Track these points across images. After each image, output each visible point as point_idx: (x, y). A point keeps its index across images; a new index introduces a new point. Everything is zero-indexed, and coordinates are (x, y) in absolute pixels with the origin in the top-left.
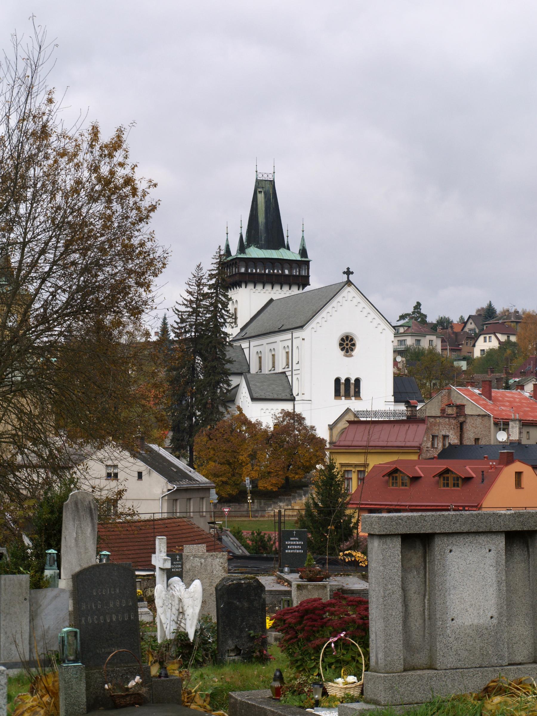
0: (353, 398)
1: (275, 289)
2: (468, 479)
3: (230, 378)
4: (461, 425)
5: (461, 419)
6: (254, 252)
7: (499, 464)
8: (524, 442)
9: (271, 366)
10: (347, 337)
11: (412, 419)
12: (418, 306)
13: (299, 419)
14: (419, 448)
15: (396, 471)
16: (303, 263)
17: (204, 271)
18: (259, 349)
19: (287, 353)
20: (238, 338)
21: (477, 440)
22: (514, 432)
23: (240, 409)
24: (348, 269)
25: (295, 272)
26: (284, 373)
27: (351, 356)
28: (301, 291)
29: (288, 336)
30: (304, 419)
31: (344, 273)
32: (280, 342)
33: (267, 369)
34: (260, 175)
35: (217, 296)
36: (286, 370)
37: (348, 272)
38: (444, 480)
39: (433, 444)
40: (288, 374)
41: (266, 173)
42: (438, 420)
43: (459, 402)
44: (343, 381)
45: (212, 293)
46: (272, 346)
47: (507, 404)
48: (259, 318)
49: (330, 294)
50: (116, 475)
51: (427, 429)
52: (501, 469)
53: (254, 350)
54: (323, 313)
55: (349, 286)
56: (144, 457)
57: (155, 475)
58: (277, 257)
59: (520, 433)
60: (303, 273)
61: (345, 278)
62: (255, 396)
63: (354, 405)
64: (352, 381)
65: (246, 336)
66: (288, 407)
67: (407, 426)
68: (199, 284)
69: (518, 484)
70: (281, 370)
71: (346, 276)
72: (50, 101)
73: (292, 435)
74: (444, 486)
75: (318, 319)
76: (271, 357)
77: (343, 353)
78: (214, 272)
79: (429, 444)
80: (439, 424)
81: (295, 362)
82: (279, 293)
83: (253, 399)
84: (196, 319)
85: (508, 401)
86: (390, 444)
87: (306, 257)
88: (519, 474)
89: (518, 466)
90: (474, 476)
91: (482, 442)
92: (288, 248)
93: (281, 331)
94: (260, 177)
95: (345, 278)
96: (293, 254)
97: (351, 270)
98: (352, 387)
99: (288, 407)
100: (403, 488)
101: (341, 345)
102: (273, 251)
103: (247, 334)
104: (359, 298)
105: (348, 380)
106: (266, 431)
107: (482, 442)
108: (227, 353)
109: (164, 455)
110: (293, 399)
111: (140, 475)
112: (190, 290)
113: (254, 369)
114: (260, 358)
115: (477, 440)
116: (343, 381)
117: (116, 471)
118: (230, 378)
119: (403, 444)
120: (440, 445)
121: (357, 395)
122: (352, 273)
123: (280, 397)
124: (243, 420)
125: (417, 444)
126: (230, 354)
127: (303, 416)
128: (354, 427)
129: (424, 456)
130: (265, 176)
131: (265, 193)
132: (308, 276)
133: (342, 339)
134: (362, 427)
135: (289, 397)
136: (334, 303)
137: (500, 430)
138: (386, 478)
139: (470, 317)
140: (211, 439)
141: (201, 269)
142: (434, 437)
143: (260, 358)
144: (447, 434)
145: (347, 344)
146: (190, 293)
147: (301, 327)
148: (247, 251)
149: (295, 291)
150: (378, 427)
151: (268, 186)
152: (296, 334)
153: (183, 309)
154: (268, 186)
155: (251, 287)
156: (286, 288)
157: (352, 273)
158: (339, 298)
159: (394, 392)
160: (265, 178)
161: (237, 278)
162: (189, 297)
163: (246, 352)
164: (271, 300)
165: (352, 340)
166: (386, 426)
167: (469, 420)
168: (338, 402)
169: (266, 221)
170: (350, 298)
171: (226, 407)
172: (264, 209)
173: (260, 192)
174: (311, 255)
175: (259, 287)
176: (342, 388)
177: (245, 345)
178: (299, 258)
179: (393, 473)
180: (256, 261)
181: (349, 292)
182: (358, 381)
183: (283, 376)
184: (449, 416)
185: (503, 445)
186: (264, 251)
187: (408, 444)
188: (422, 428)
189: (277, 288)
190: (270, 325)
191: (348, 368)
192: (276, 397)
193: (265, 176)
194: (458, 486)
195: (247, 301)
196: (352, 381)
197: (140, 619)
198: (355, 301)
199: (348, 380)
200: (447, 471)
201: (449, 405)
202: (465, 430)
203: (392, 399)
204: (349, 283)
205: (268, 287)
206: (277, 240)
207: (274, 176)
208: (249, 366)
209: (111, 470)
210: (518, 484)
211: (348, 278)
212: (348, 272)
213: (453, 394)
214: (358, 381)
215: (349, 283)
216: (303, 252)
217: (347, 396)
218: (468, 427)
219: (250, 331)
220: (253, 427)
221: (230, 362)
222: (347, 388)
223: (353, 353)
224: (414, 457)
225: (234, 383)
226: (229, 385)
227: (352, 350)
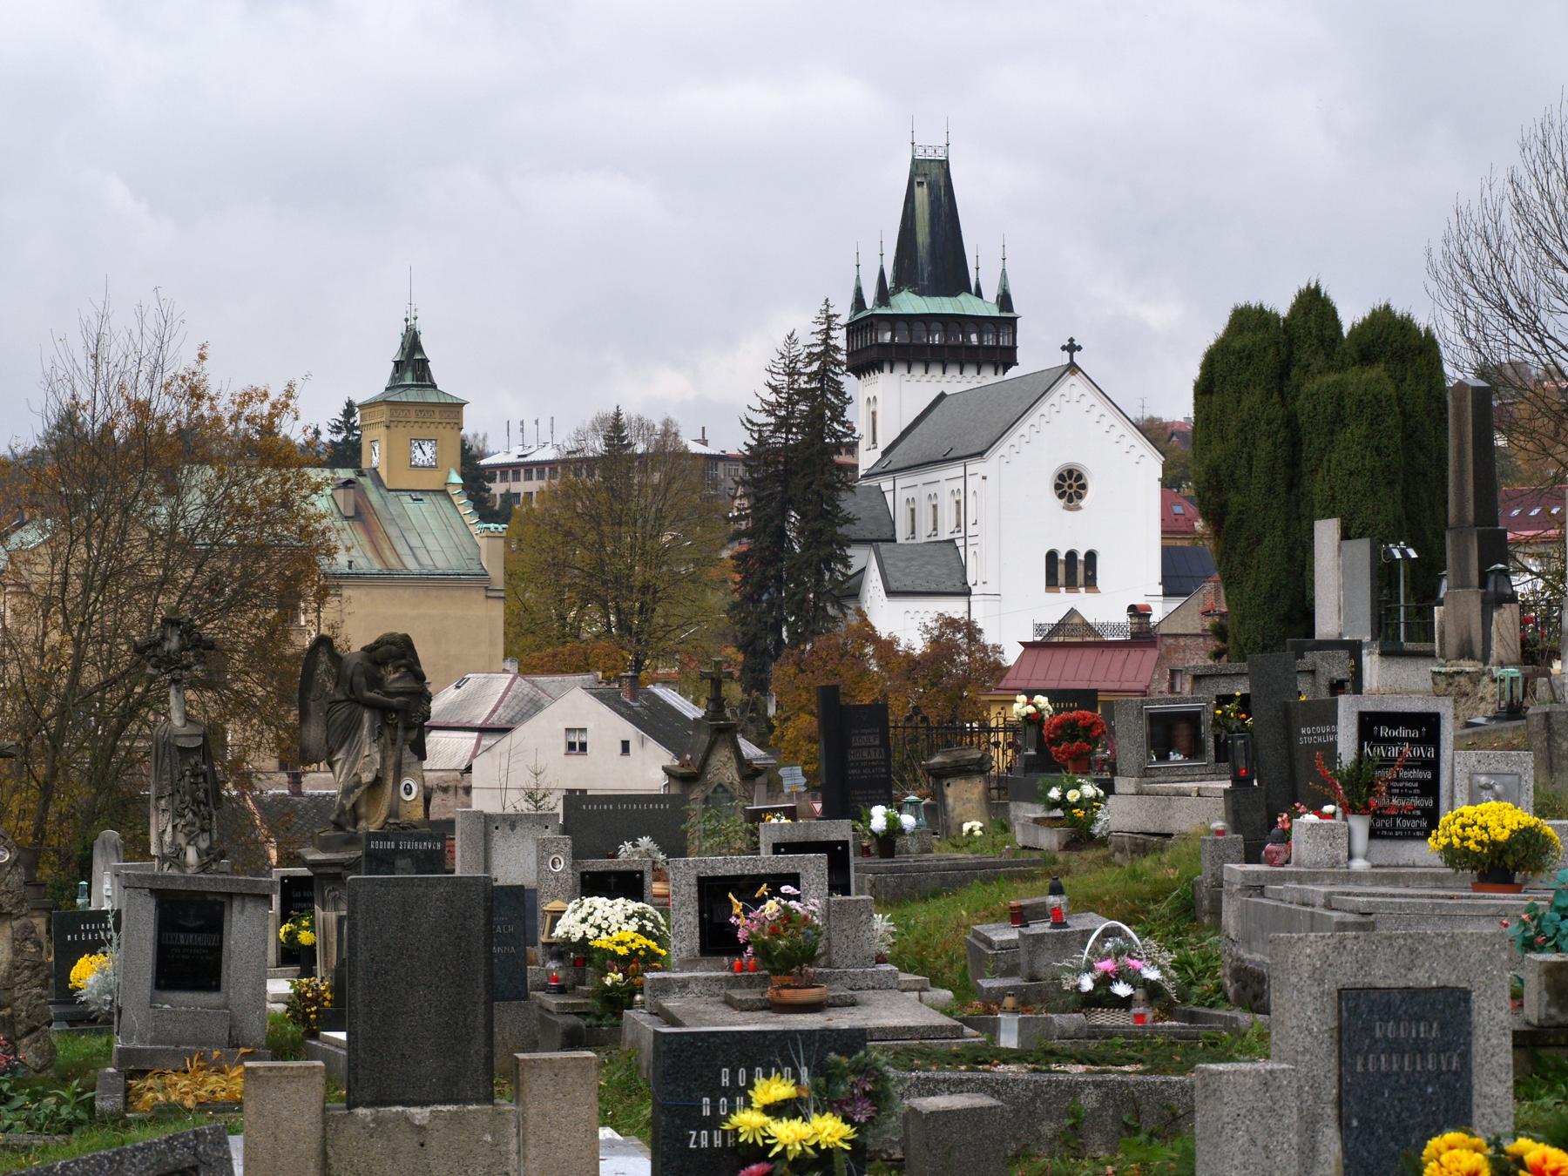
0: (1082, 590)
1: (949, 374)
3: (849, 552)
6: (909, 303)
9: (931, 527)
10: (1070, 472)
13: (972, 631)
17: (799, 346)
19: (958, 502)
20: (876, 470)
23: (861, 614)
24: (1071, 340)
25: (989, 340)
26: (952, 541)
27: (1078, 508)
28: (1000, 378)
29: (957, 470)
30: (980, 631)
31: (1064, 348)
33: (922, 537)
34: (920, 151)
35: (823, 395)
36: (956, 535)
37: (1071, 347)
40: (960, 543)
41: (931, 144)
44: (1062, 557)
45: (813, 390)
46: (932, 489)
48: (917, 430)
49: (1047, 383)
50: (583, 747)
51: (1161, 658)
53: (902, 496)
54: (1023, 428)
55: (1073, 373)
56: (637, 713)
57: (652, 744)
58: (951, 311)
60: (1004, 341)
61: (1065, 358)
62: (894, 586)
64: (1081, 557)
65: (890, 467)
66: (954, 608)
68: (792, 373)
70: (947, 536)
71: (1067, 354)
72: (202, 357)
73: (957, 665)
75: (1013, 438)
76: (931, 510)
77: (1062, 502)
78: (816, 350)
79: (1165, 686)
81: (970, 521)
82: (956, 382)
83: (891, 593)
84: (787, 439)
87: (1011, 310)
93: (947, 460)
94: (920, 155)
95: (1065, 358)
96: (986, 307)
97: (1076, 343)
98: (1081, 569)
99: (954, 608)
100: (412, 396)
101: (1057, 487)
102: (945, 299)
103: (888, 467)
104: (1092, 397)
105: (1071, 555)
106: (908, 656)
108: (842, 505)
109: (679, 708)
110: (967, 593)
111: (625, 747)
112: (774, 383)
113: (902, 535)
114: (913, 510)
116: (1062, 557)
117: (583, 739)
118: (849, 552)
119: (1116, 687)
121: (1091, 582)
122: (1079, 348)
123: (942, 588)
124: (867, 633)
125: (1141, 686)
126: (848, 503)
127: (979, 626)
130: (930, 151)
131: (929, 185)
132: (1013, 348)
133: (1061, 477)
134: (1060, 655)
135: (959, 588)
136: (1044, 407)
140: (803, 671)
141: (796, 342)
142: (1173, 673)
143: (913, 510)
145: (1070, 486)
146: (775, 389)
147: (981, 454)
148: (893, 300)
149: (989, 377)
151: (936, 171)
152: (974, 467)
153: (762, 418)
154: (936, 171)
155: (901, 370)
156: (970, 372)
157: (1079, 348)
158: (1054, 397)
159: (1163, 577)
161: (874, 354)
162: (773, 398)
163: (889, 497)
164: (942, 396)
165: (1080, 477)
169: (932, 240)
170: (1075, 397)
171: (841, 608)
172: (927, 217)
173: (921, 184)
174: (1018, 307)
175: (918, 371)
176: (1061, 570)
177: (886, 485)
178: (995, 312)
180: (910, 319)
181: (1072, 386)
182: (1091, 556)
183: (950, 547)
186: (928, 299)
187: (1126, 686)
188: (1152, 655)
189: (953, 372)
190: (935, 446)
191: (1070, 532)
192: (933, 588)
193: (930, 151)
195: (885, 404)
196: (1081, 557)
197: (1434, 1143)
198: (1085, 403)
199: (1071, 555)
203: (1160, 589)
204: (1073, 368)
205: (936, 371)
207: (947, 151)
208: (893, 523)
209: (575, 738)
211: (1071, 358)
212: (1071, 347)
215: (1073, 368)
216: (1005, 301)
217: (1071, 585)
219: (898, 458)
220: (887, 648)
221: (849, 521)
222: (1073, 570)
223: (1082, 503)
225: (856, 564)
226: (848, 567)
227: (1080, 497)
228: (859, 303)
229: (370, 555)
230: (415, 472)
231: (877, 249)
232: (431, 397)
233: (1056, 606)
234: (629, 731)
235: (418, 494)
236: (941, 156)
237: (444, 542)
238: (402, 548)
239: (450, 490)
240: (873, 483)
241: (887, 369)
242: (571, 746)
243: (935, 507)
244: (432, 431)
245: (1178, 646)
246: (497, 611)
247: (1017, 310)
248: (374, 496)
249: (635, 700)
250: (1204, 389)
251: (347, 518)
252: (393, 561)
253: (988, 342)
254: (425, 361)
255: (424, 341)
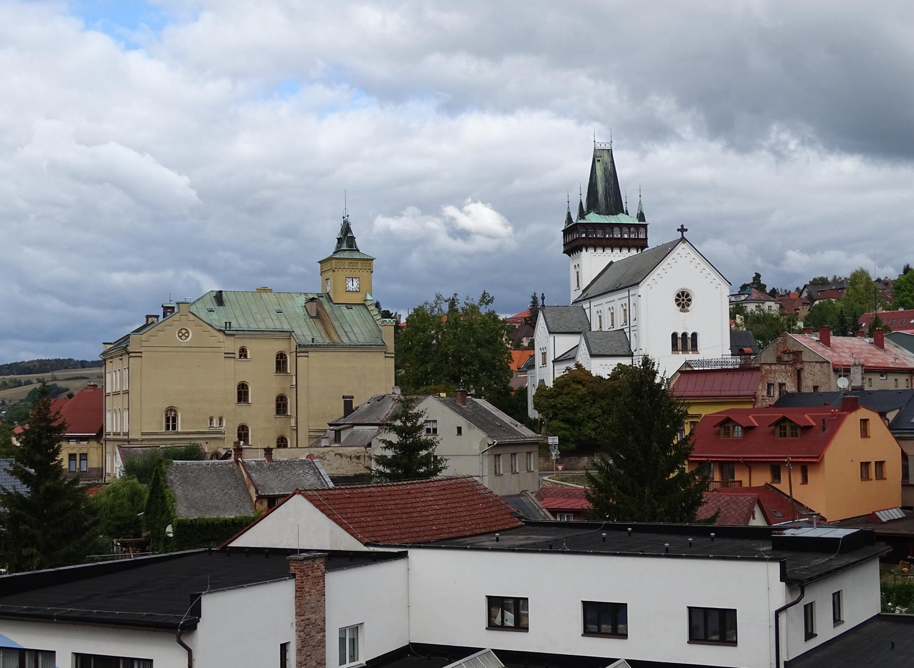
2: (808, 428)
4: (799, 372)
5: (799, 366)
6: (593, 218)
7: (842, 411)
8: (867, 388)
10: (683, 293)
11: (744, 369)
12: (758, 276)
14: (755, 396)
15: (728, 420)
16: (641, 226)
18: (598, 308)
19: (625, 310)
21: (816, 388)
22: (857, 378)
24: (682, 226)
31: (678, 230)
32: (617, 300)
34: (598, 145)
37: (682, 230)
38: (781, 429)
39: (769, 392)
42: (773, 367)
43: (795, 349)
44: (680, 336)
46: (610, 305)
47: (847, 350)
48: (600, 279)
49: (665, 251)
52: (844, 417)
53: (594, 310)
55: (684, 242)
59: (863, 378)
60: (641, 236)
62: (594, 352)
63: (690, 356)
64: (689, 336)
67: (741, 374)
69: (865, 433)
74: (781, 436)
77: (679, 308)
79: (765, 393)
80: (775, 371)
82: (618, 256)
85: (848, 348)
86: (723, 394)
88: (864, 422)
89: (863, 413)
90: (814, 424)
91: (822, 390)
92: (627, 214)
98: (689, 342)
100: (346, 255)
105: (684, 335)
107: (822, 390)
110: (631, 355)
111: (459, 430)
113: (595, 327)
115: (816, 388)
116: (680, 336)
117: (435, 426)
119: (737, 393)
120: (777, 394)
122: (686, 230)
123: (619, 353)
125: (751, 393)
128: (686, 376)
129: (759, 405)
130: (603, 145)
132: (646, 239)
134: (693, 377)
137: (840, 376)
138: (718, 428)
139: (805, 286)
142: (770, 385)
144: (784, 381)
145: (683, 300)
150: (711, 376)
155: (591, 251)
157: (686, 230)
158: (674, 254)
160: (603, 147)
164: (612, 263)
165: (688, 295)
166: (719, 375)
167: (806, 367)
168: (676, 356)
175: (600, 251)
176: (680, 342)
177: (586, 305)
179: (726, 423)
181: (682, 248)
182: (694, 335)
184: (785, 363)
185: (846, 392)
189: (617, 251)
191: (684, 323)
192: (614, 353)
193: (603, 145)
194: (796, 436)
196: (689, 336)
199: (684, 335)
200: (784, 419)
201: (784, 352)
202: (803, 378)
203: (730, 352)
204: (683, 240)
205: (608, 251)
206: (617, 207)
210: (865, 433)
212: (682, 230)
213: (790, 342)
214: (694, 335)
216: (641, 216)
217: (685, 350)
218: (805, 374)
219: (591, 292)
222: (684, 342)
224: (750, 407)
227: (688, 305)
228: (569, 219)
229: (324, 336)
230: (349, 294)
231: (580, 193)
232: (356, 255)
233: (680, 360)
234: (462, 421)
235: (349, 306)
236: (608, 147)
237: (363, 329)
238: (341, 332)
239: (367, 303)
240: (579, 305)
241: (584, 250)
242: (865, 465)
243: (612, 314)
244: (357, 273)
245: (771, 370)
246: (391, 363)
247: (647, 221)
248: (327, 307)
249: (465, 404)
250: (197, 612)
251: (312, 317)
252: (336, 339)
253: (633, 237)
254: (353, 238)
255: (352, 227)
